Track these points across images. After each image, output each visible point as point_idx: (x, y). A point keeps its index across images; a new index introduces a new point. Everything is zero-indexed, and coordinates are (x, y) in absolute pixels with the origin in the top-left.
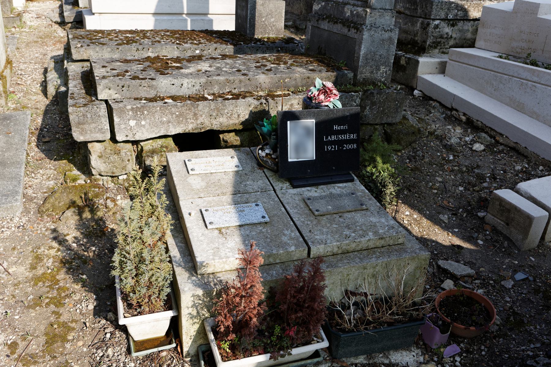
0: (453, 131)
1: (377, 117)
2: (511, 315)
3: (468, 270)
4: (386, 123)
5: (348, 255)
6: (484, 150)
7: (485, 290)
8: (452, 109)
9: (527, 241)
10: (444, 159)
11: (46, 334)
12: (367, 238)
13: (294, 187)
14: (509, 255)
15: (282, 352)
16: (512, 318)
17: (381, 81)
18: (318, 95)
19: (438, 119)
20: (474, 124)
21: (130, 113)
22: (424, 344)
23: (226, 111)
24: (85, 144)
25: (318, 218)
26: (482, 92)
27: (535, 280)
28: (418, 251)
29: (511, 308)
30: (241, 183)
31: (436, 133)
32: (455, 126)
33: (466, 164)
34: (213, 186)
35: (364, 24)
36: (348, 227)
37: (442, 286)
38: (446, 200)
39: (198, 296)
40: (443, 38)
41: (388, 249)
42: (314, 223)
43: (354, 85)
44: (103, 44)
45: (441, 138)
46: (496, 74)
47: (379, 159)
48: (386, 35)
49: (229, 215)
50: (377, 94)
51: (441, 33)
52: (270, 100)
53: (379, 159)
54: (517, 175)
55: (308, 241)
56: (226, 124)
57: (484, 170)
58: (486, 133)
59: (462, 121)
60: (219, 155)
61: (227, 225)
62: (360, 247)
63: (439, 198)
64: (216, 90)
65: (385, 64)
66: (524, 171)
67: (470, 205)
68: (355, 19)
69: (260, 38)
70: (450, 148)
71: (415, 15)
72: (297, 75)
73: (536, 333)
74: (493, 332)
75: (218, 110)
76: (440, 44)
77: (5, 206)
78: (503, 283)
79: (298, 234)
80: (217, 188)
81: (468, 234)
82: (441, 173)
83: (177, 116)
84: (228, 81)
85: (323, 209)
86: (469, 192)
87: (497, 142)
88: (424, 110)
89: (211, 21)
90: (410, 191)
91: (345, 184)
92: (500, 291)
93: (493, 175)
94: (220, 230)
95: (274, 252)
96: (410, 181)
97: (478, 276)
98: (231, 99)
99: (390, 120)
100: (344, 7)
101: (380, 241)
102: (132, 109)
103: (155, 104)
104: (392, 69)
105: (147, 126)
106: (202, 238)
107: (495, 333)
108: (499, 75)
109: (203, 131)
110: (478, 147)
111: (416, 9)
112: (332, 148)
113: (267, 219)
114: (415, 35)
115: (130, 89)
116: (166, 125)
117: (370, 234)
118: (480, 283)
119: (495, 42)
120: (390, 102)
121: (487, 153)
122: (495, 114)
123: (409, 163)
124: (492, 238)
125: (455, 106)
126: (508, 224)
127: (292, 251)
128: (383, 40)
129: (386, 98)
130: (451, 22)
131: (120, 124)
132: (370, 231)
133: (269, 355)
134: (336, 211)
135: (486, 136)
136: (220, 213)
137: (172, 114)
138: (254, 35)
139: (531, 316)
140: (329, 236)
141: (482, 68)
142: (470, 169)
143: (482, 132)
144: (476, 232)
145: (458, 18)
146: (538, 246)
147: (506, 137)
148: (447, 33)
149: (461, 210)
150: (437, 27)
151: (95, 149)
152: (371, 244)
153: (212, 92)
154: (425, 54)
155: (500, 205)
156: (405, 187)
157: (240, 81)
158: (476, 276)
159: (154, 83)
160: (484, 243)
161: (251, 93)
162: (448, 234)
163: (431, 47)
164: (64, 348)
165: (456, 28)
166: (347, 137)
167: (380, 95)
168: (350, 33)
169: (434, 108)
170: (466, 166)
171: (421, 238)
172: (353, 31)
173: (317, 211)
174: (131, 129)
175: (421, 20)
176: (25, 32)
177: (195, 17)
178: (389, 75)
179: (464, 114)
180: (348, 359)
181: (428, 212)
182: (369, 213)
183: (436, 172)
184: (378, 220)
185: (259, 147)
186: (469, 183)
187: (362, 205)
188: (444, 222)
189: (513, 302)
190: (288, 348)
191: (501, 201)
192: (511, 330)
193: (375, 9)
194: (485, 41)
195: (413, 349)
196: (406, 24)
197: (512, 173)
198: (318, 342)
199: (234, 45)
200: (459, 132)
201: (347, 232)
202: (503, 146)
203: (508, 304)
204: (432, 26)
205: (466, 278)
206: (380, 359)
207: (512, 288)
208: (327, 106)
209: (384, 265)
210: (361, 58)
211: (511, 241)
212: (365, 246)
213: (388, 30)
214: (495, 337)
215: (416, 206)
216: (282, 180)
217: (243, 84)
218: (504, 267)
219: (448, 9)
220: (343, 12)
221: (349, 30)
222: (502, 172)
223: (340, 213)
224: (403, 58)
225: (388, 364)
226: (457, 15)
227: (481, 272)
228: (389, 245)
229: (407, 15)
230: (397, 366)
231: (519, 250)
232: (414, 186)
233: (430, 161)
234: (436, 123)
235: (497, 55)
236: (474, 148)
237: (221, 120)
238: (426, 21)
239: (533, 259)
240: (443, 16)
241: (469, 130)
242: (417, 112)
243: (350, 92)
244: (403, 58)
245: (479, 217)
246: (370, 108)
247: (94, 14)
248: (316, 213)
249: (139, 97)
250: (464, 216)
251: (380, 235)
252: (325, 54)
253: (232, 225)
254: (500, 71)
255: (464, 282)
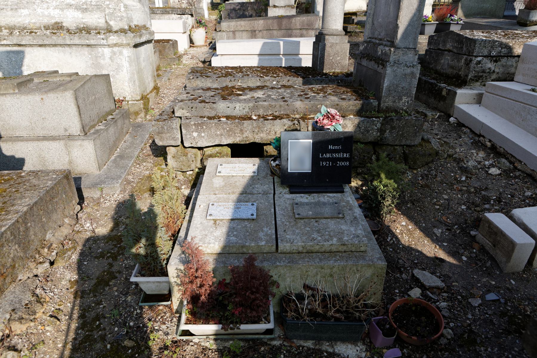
0: (476, 155)
1: (396, 140)
2: (466, 332)
3: (439, 283)
4: (404, 145)
5: (311, 254)
6: (500, 174)
7: (450, 304)
8: (480, 136)
9: (510, 264)
10: (456, 179)
11: (98, 278)
12: (330, 243)
13: (291, 193)
14: (489, 274)
15: (231, 326)
16: (466, 336)
17: (402, 110)
18: (323, 119)
19: (465, 143)
20: (497, 150)
21: (194, 127)
22: (371, 342)
23: (265, 129)
24: (165, 147)
25: (297, 220)
26: (511, 122)
27: (506, 303)
28: (376, 260)
29: (469, 325)
30: (251, 186)
31: (454, 156)
32: (479, 150)
33: (476, 186)
34: (229, 186)
35: (388, 61)
36: (318, 231)
37: (409, 293)
38: (446, 216)
39: (181, 270)
40: (485, 73)
41: (349, 254)
42: (292, 224)
43: (378, 112)
44: (207, 77)
45: (458, 161)
46: (525, 105)
47: (383, 176)
48: (409, 71)
49: (227, 210)
50: (397, 120)
51: (484, 68)
52: (301, 122)
53: (383, 176)
54: (524, 201)
55: (279, 239)
56: (265, 139)
57: (491, 193)
58: (507, 159)
59: (486, 146)
60: (246, 163)
61: (222, 218)
62: (323, 250)
63: (440, 214)
64: (261, 112)
65: (407, 95)
66: (533, 198)
67: (466, 223)
68: (384, 57)
69: (328, 72)
70: (465, 170)
71: (461, 53)
72: (328, 102)
73: (485, 355)
74: (441, 345)
75: (259, 127)
76: (481, 77)
77: (110, 186)
78: (470, 300)
79: (274, 232)
80: (231, 188)
81: (455, 249)
82: (449, 191)
83: (228, 131)
84: (271, 106)
85: (304, 214)
86: (470, 211)
87: (515, 168)
88: (455, 135)
89: (300, 60)
90: (414, 204)
91: (335, 194)
92: (465, 307)
93: (499, 198)
94: (215, 221)
95: (247, 244)
96: (417, 196)
97: (449, 289)
98: (271, 119)
99: (408, 142)
100: (377, 47)
101: (343, 247)
102: (195, 124)
103: (212, 121)
104: (413, 99)
105: (206, 137)
106: (198, 226)
107: (443, 346)
108: (528, 106)
109: (247, 143)
110: (494, 171)
111: (462, 48)
112: (326, 164)
113: (255, 217)
114: (460, 70)
115: (197, 109)
116: (219, 137)
117: (335, 239)
118: (448, 297)
119: (533, 76)
120: (409, 127)
121: (502, 177)
122: (516, 143)
123: (421, 180)
124: (477, 257)
125: (482, 133)
126: (494, 246)
127: (262, 245)
128: (405, 75)
129: (406, 124)
130: (494, 59)
131: (186, 135)
132: (335, 237)
133: (221, 326)
134: (314, 217)
135: (506, 161)
136: (222, 208)
137: (224, 129)
138: (323, 70)
139: (486, 337)
140: (298, 237)
141: (513, 100)
142: (478, 191)
143: (503, 158)
144: (463, 249)
145: (502, 54)
146: (524, 271)
147: (524, 164)
148: (489, 69)
149: (456, 227)
150: (479, 62)
151: (171, 151)
152: (334, 249)
153: (258, 114)
154: (466, 87)
155: (489, 227)
156: (411, 200)
157: (281, 106)
158: (445, 289)
159: (214, 105)
160: (468, 259)
161: (288, 115)
162: (436, 247)
163: (473, 80)
164: (104, 290)
165: (499, 63)
166: (340, 155)
167: (400, 121)
168: (378, 69)
169: (465, 133)
170: (475, 188)
171: (408, 247)
172: (381, 67)
173: (298, 214)
174: (194, 139)
175: (465, 57)
176: (180, 68)
177: (288, 57)
178: (411, 104)
179: (490, 141)
180: (299, 341)
181: (424, 225)
182: (343, 221)
183: (444, 190)
184: (347, 228)
185: (272, 159)
186: (473, 203)
187: (339, 214)
188: (436, 236)
189: (475, 320)
190: (237, 323)
191: (490, 223)
192: (460, 346)
193: (399, 48)
194: (523, 75)
195: (359, 345)
196: (452, 61)
197: (519, 198)
198: (265, 323)
199: (303, 78)
200: (481, 156)
201: (315, 235)
202: (520, 173)
203: (468, 321)
204: (475, 62)
205: (435, 290)
206: (326, 347)
207: (478, 307)
208: (329, 129)
209: (340, 268)
210: (384, 89)
211: (496, 261)
212: (328, 249)
213: (410, 66)
214: (441, 350)
215: (414, 219)
216: (284, 186)
217: (282, 108)
218: (479, 285)
219: (492, 47)
220: (376, 52)
221: (378, 67)
222: (509, 196)
223: (317, 218)
224: (445, 89)
225: (331, 353)
226: (500, 52)
227: (453, 286)
228: (352, 251)
229: (454, 53)
230: (338, 356)
231: (501, 271)
232: (418, 201)
233: (442, 180)
234: (461, 147)
235: (530, 87)
236: (490, 172)
237: (262, 135)
238: (469, 58)
239: (513, 283)
240: (486, 53)
241: (492, 155)
242: (448, 136)
243: (372, 117)
244: (445, 89)
245: (471, 236)
246: (390, 132)
247: (217, 55)
248: (297, 216)
249: (204, 115)
250: (458, 232)
251: (343, 241)
252: (363, 86)
253: (226, 218)
254: (528, 103)
255: (431, 293)
